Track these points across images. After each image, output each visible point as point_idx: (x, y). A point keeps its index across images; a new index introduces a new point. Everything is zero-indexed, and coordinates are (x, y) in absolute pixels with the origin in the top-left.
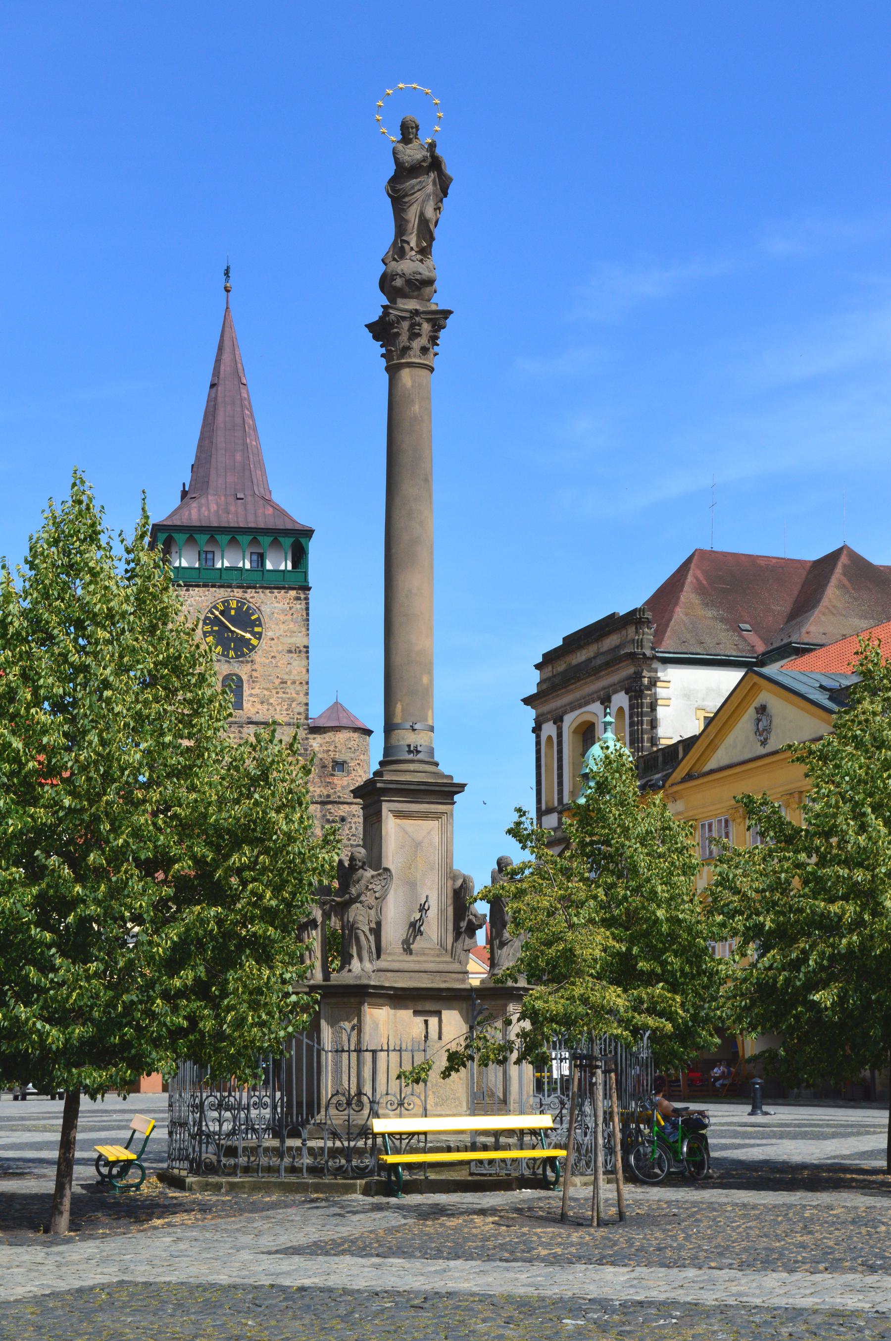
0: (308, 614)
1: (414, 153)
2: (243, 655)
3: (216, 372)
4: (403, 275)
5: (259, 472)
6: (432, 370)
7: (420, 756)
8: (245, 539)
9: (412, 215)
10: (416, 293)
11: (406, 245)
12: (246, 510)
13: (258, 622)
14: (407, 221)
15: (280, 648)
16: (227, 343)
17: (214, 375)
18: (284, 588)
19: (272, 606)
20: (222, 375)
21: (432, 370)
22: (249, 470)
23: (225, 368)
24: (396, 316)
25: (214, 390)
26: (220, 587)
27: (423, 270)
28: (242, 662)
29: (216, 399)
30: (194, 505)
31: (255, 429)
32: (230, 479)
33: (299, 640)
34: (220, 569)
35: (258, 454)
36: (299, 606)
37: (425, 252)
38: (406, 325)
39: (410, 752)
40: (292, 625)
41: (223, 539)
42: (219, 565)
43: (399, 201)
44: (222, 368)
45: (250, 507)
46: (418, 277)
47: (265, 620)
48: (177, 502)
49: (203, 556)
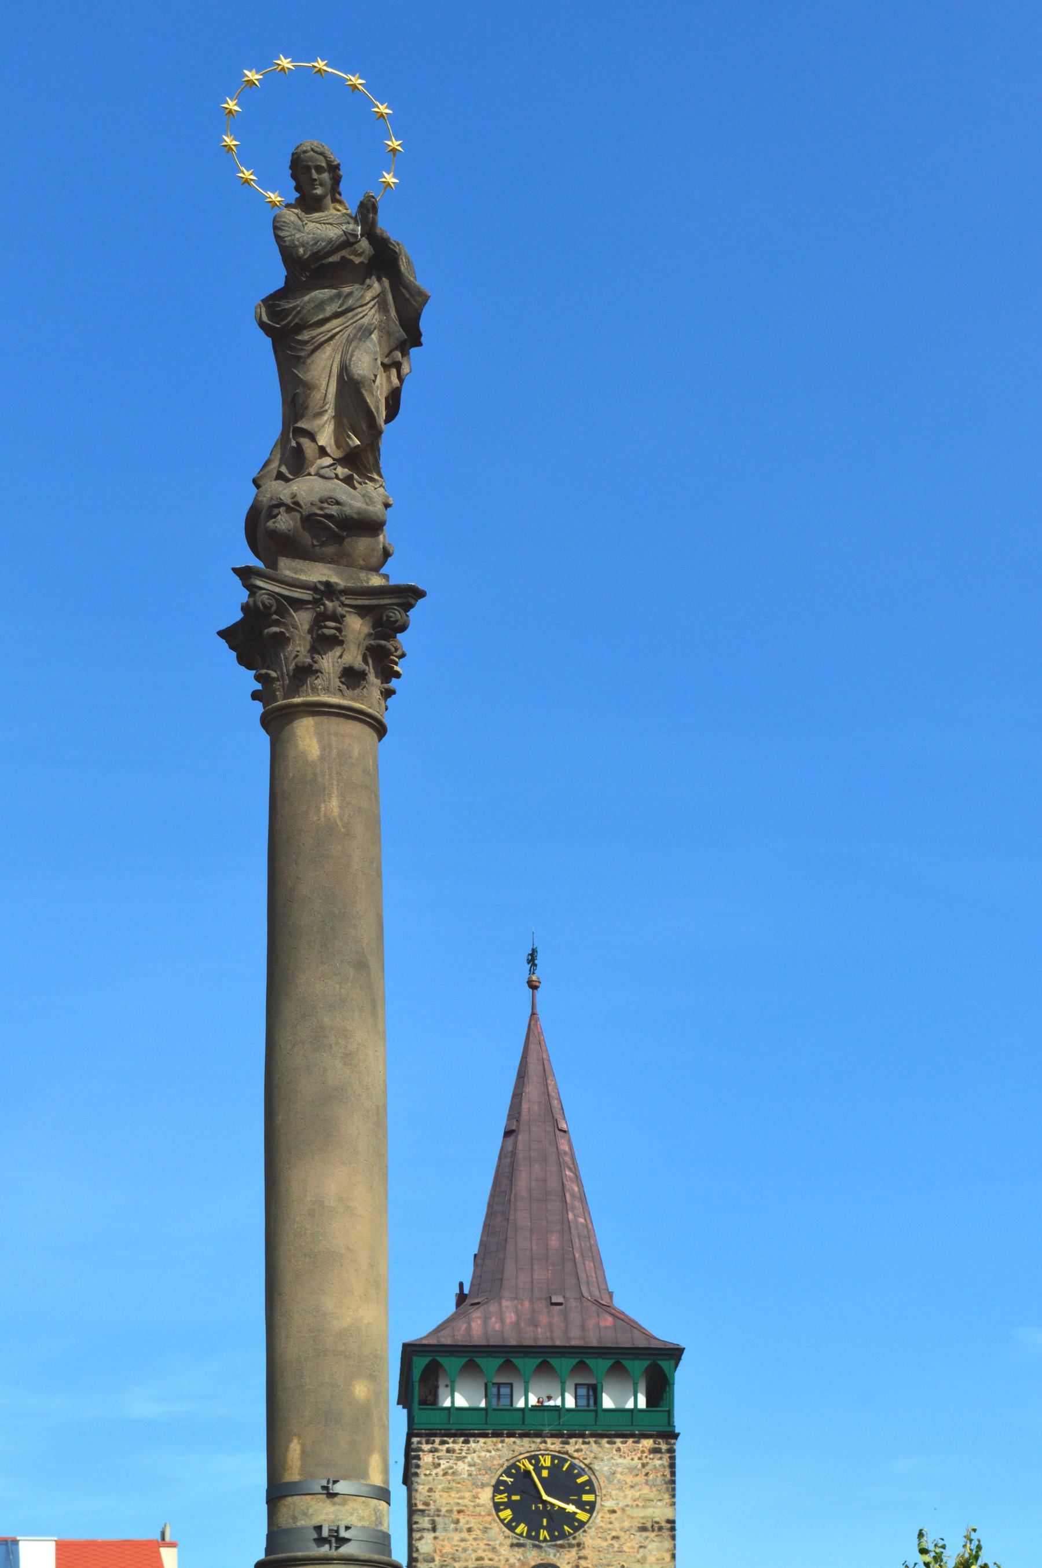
0: (673, 1474)
1: (326, 227)
2: (563, 1536)
3: (515, 1111)
4: (293, 507)
5: (589, 1264)
6: (380, 729)
7: (346, 1550)
8: (565, 1364)
9: (322, 372)
10: (330, 550)
11: (305, 442)
12: (566, 1319)
13: (590, 1487)
14: (309, 387)
15: (627, 1524)
16: (533, 1067)
17: (510, 1117)
18: (632, 1436)
19: (616, 1467)
20: (524, 1116)
21: (380, 729)
22: (573, 1259)
23: (530, 1105)
24: (272, 594)
25: (511, 1140)
26: (522, 1436)
27: (356, 499)
28: (562, 1546)
29: (514, 1153)
30: (477, 1314)
31: (583, 1198)
32: (540, 1274)
33: (660, 1512)
34: (522, 1410)
35: (588, 1234)
36: (658, 1463)
37: (360, 462)
38: (303, 619)
39: (321, 1541)
40: (646, 1490)
41: (527, 1364)
42: (520, 1404)
43: (286, 331)
44: (525, 1106)
45: (575, 1317)
46: (333, 510)
47: (601, 1482)
48: (451, 1308)
49: (494, 1390)
